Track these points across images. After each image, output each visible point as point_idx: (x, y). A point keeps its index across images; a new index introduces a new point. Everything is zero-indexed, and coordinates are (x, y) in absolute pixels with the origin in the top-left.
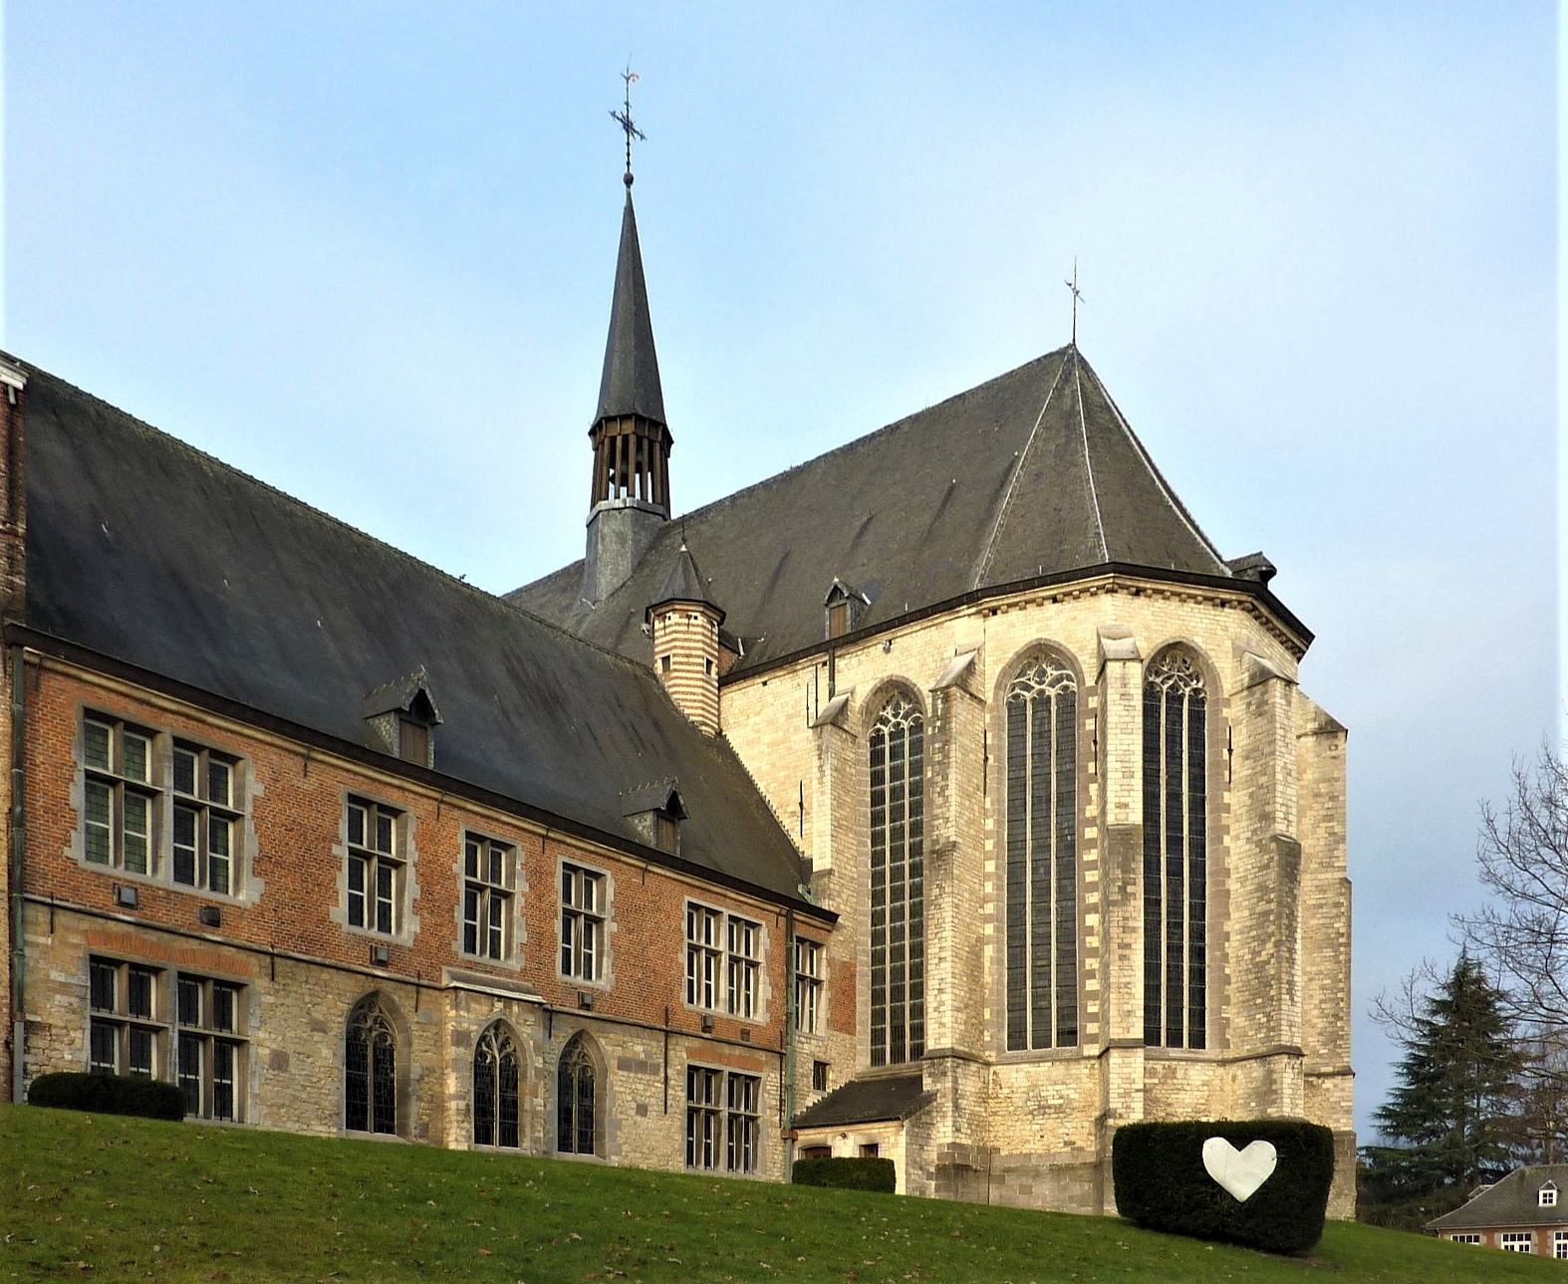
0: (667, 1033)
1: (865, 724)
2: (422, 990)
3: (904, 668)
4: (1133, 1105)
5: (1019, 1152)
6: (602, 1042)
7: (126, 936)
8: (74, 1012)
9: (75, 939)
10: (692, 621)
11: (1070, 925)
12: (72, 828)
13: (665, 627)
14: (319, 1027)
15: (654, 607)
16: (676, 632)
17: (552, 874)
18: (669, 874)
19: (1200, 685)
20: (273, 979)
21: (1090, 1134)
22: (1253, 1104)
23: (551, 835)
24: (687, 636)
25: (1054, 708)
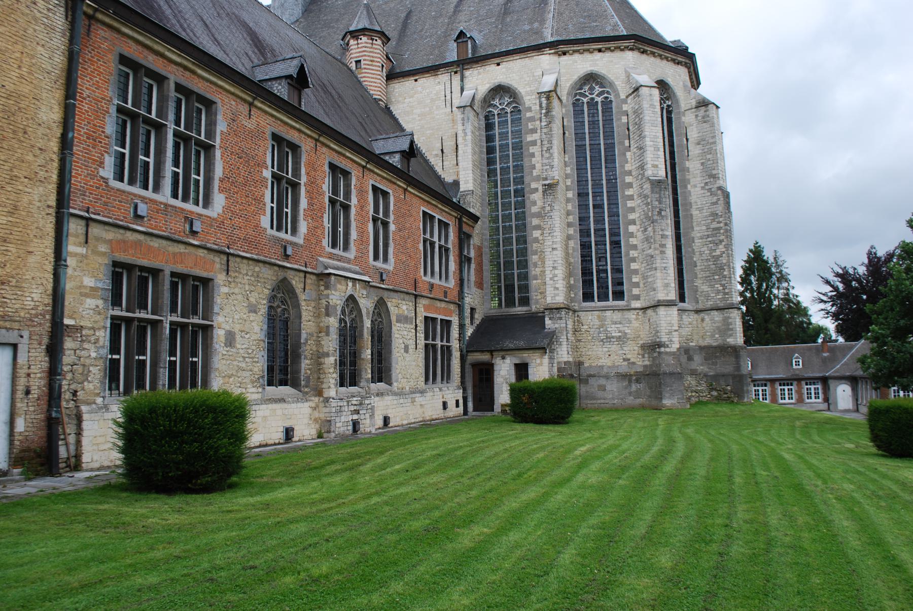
0: (416, 296)
1: (482, 107)
2: (308, 275)
3: (509, 79)
4: (673, 339)
5: (595, 364)
6: (389, 304)
7: (138, 244)
8: (99, 314)
9: (103, 248)
10: (374, 42)
11: (617, 230)
12: (106, 152)
13: (358, 44)
14: (253, 309)
15: (351, 32)
16: (366, 47)
17: (367, 192)
18: (416, 193)
19: (670, 103)
20: (228, 274)
21: (639, 354)
22: (717, 336)
23: (368, 166)
24: (372, 50)
25: (600, 108)
